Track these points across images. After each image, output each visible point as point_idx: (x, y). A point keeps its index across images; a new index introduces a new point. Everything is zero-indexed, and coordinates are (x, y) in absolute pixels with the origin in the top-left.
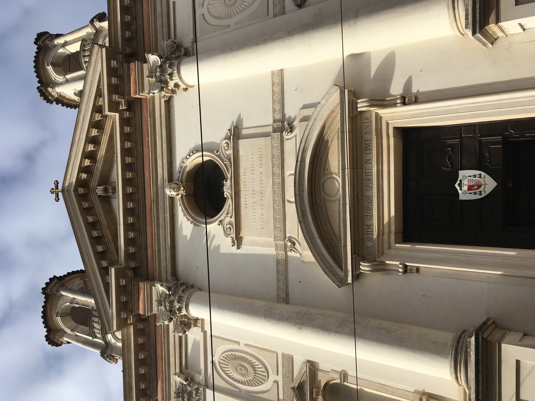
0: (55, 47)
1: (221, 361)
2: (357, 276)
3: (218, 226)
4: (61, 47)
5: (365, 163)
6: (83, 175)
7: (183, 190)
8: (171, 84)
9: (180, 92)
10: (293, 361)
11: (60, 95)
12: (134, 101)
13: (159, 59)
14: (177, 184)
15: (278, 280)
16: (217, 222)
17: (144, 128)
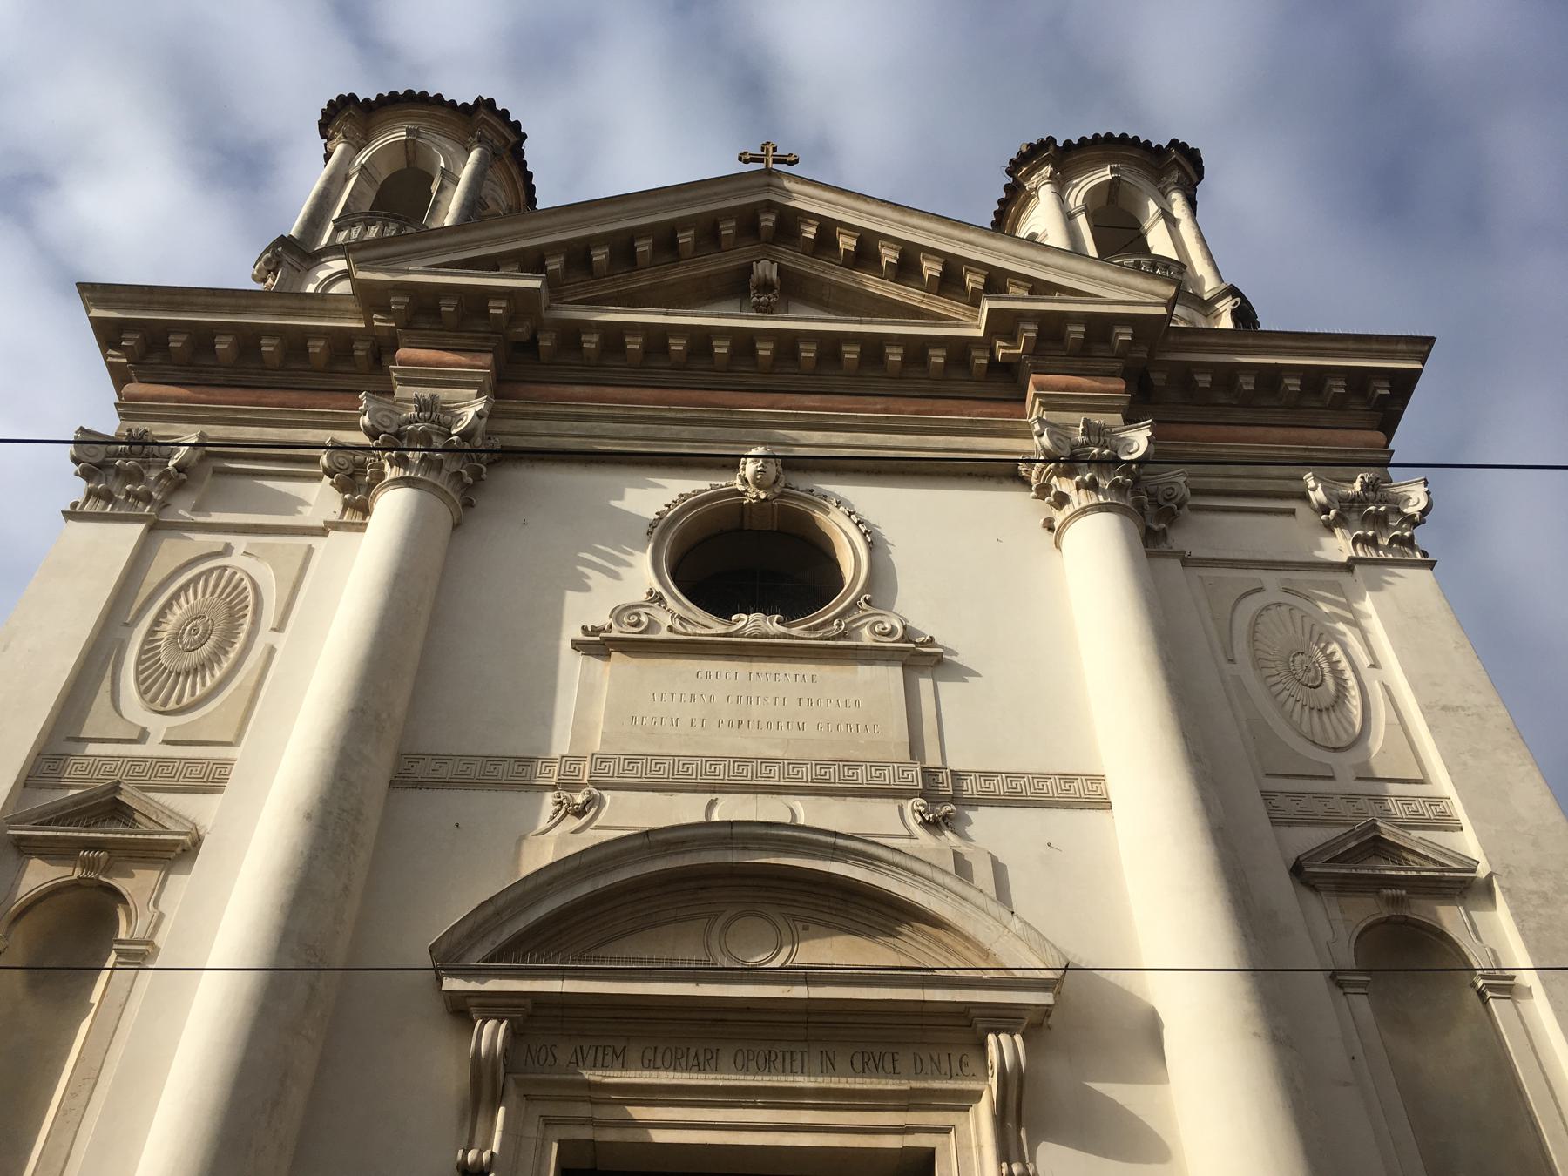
0: (1162, 194)
1: (227, 574)
2: (463, 1011)
3: (648, 590)
4: (1162, 209)
5: (822, 1052)
6: (814, 230)
7: (758, 497)
8: (1065, 486)
9: (1043, 508)
10: (205, 792)
11: (1029, 197)
12: (1016, 381)
13: (1134, 457)
14: (775, 482)
15: (469, 759)
16: (658, 588)
17: (940, 404)
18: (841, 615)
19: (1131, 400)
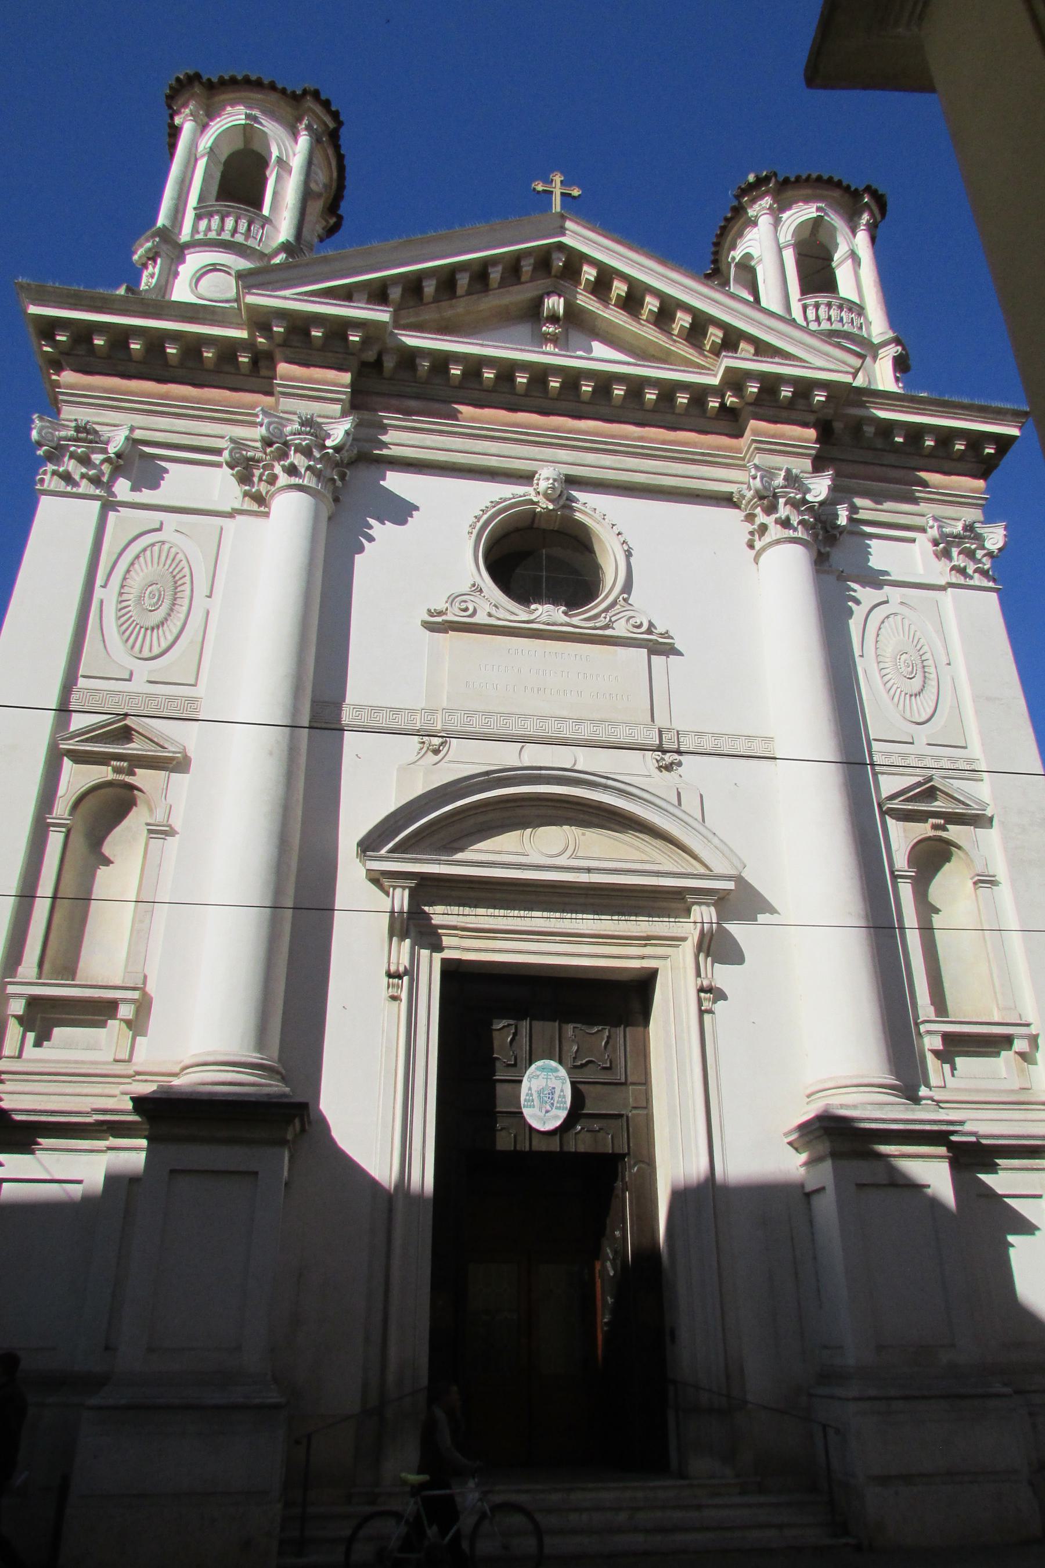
12: (737, 421)
14: (560, 495)
18: (606, 610)
19: (819, 450)
